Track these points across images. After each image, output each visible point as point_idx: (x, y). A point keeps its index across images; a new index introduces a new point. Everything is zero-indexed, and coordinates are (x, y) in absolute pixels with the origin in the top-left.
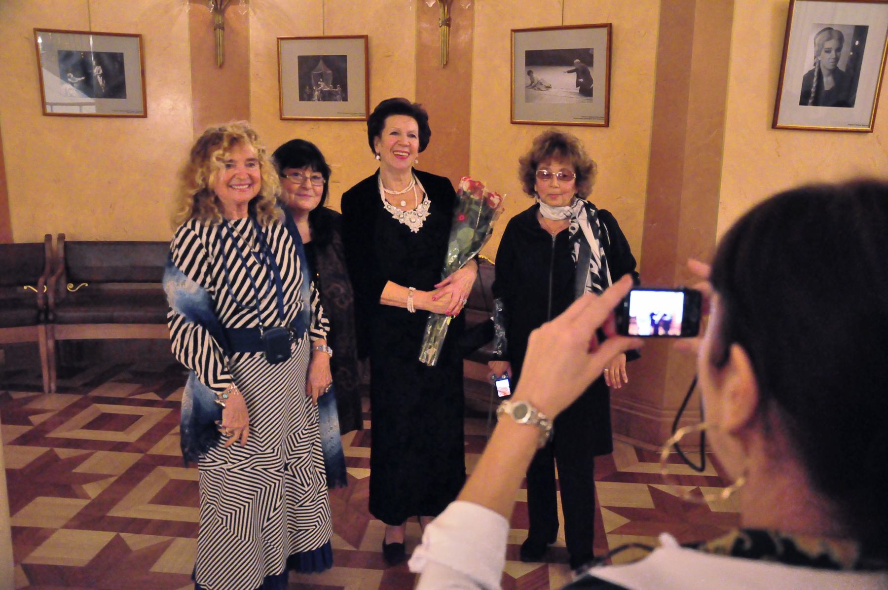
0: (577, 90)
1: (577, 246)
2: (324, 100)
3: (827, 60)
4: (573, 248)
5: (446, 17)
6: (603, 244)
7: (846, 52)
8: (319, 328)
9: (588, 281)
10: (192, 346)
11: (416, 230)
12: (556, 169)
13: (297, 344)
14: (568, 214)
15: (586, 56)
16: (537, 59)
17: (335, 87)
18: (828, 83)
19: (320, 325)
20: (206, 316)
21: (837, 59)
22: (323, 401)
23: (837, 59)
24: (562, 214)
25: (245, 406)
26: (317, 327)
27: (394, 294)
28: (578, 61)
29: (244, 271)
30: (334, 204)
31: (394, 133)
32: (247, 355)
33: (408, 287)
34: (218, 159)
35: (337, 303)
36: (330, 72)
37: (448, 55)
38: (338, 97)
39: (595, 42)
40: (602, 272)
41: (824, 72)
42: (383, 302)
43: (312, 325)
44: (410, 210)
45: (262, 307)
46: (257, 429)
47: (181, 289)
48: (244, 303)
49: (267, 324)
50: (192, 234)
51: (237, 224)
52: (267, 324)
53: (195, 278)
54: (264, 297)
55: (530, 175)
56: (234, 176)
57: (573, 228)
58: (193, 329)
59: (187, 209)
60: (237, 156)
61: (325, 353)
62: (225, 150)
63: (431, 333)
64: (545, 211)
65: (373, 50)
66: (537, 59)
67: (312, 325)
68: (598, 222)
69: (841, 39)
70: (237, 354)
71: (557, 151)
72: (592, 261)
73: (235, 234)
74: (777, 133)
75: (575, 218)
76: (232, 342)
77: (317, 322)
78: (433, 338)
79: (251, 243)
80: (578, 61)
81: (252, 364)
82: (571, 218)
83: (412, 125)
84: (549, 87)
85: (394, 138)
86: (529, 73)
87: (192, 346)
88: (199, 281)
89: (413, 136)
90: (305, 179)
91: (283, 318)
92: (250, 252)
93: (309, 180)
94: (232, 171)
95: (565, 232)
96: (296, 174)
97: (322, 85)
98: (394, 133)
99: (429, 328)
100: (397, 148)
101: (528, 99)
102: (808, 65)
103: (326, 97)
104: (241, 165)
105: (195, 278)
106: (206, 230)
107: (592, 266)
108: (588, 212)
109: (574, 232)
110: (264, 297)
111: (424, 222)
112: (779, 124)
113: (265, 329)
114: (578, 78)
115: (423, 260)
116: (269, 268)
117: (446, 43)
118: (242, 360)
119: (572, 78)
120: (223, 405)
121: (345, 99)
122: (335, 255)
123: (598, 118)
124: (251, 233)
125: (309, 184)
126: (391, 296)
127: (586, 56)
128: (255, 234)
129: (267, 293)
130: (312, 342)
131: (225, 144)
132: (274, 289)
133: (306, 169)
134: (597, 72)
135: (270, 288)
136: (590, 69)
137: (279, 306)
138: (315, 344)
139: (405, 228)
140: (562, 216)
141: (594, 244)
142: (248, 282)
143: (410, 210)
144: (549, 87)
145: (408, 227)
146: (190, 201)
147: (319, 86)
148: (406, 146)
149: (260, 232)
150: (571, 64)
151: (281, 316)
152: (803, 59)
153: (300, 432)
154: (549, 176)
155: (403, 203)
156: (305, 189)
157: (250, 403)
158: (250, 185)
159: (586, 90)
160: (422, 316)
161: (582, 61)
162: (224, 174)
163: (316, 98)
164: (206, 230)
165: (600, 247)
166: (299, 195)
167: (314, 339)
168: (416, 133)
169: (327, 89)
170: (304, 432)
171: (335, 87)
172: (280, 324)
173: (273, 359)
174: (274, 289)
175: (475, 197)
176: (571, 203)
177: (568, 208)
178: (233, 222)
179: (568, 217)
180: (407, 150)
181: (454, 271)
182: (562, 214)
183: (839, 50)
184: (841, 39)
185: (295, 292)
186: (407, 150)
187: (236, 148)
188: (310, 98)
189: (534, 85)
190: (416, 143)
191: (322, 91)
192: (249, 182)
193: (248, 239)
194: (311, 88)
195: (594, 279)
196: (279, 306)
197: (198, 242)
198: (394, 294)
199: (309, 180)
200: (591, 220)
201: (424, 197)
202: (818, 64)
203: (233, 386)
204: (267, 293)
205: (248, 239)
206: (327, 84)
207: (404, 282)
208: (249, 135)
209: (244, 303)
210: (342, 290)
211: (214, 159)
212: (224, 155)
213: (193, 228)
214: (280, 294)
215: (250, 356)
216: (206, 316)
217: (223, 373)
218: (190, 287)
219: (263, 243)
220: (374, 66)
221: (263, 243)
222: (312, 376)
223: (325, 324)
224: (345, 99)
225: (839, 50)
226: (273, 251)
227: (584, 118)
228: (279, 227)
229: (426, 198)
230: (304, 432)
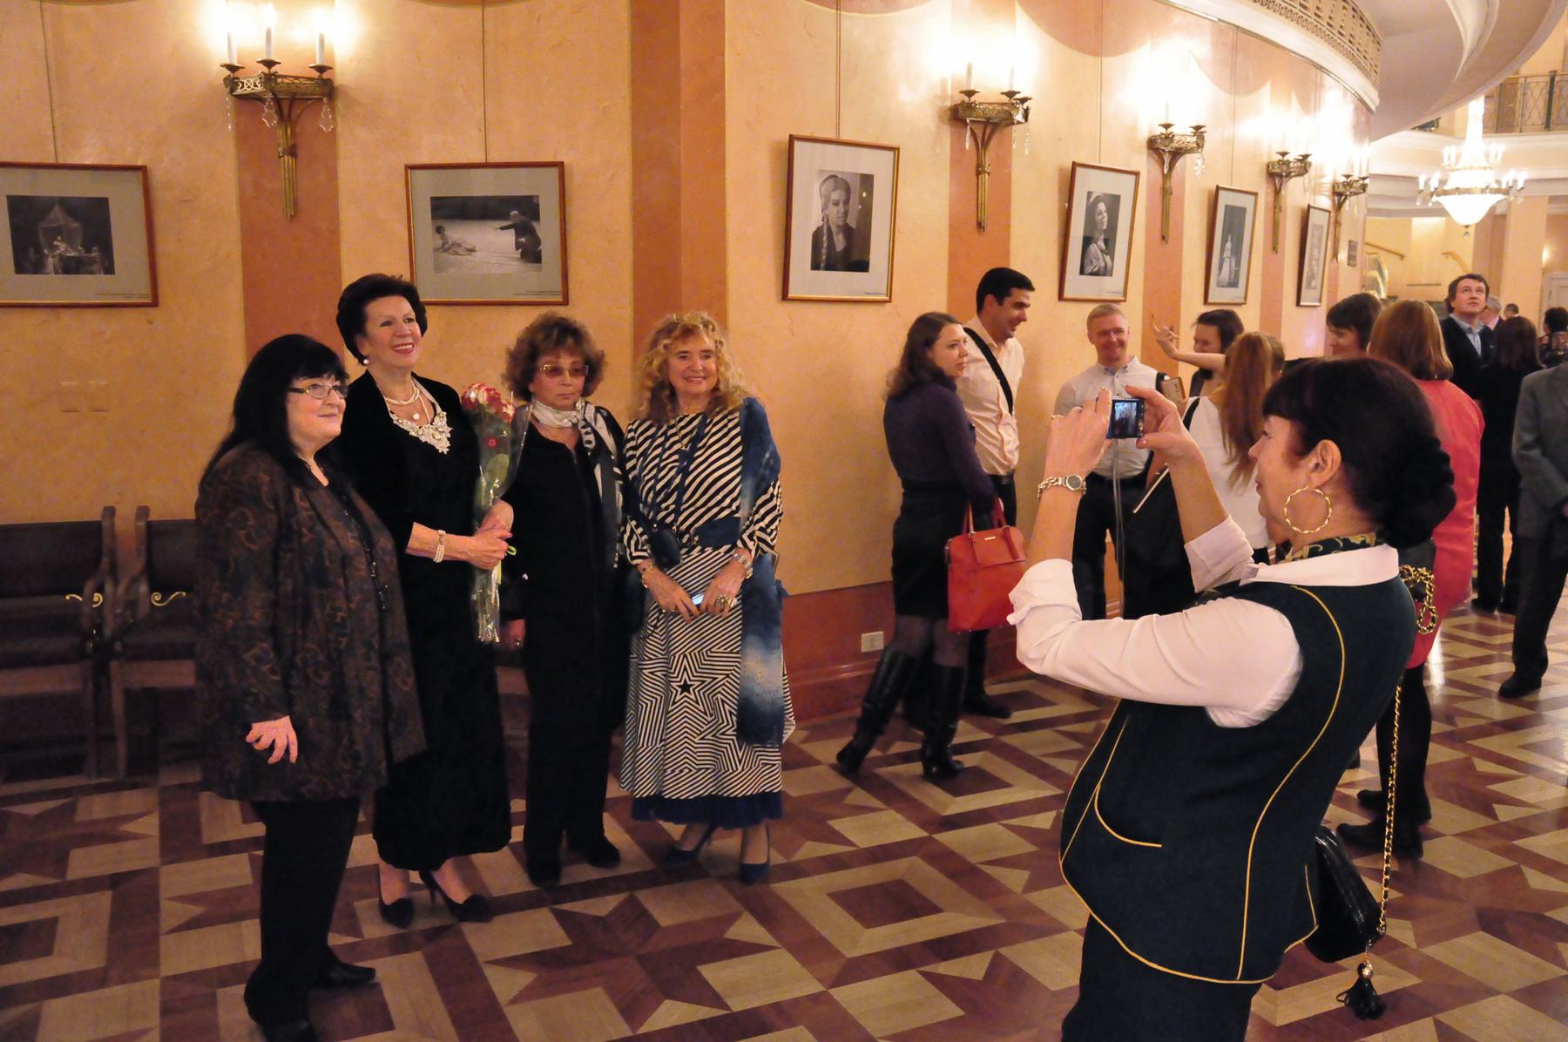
0: (518, 254)
2: (67, 271)
3: (835, 213)
5: (291, 142)
7: (855, 206)
11: (446, 451)
12: (566, 362)
13: (702, 551)
15: (529, 207)
16: (450, 210)
17: (88, 250)
18: (840, 243)
21: (846, 213)
23: (846, 213)
28: (520, 214)
31: (387, 324)
36: (76, 225)
37: (295, 203)
38: (95, 267)
39: (542, 186)
41: (834, 229)
42: (408, 551)
59: (646, 404)
60: (691, 346)
65: (159, 195)
66: (450, 210)
69: (848, 190)
71: (570, 340)
74: (787, 305)
80: (520, 214)
83: (406, 307)
84: (472, 251)
86: (439, 230)
89: (410, 320)
97: (62, 247)
98: (387, 324)
101: (438, 268)
102: (815, 221)
103: (71, 267)
112: (790, 295)
114: (518, 235)
117: (293, 184)
119: (509, 238)
121: (109, 269)
123: (551, 293)
127: (529, 207)
134: (547, 228)
136: (535, 224)
139: (430, 448)
144: (472, 251)
146: (648, 394)
147: (53, 248)
150: (505, 216)
152: (810, 214)
154: (556, 371)
159: (531, 253)
161: (522, 213)
163: (51, 268)
168: (413, 315)
169: (72, 254)
171: (88, 250)
180: (410, 340)
183: (847, 202)
184: (848, 190)
188: (38, 268)
189: (446, 247)
191: (62, 257)
193: (685, 436)
194: (39, 251)
202: (826, 218)
205: (685, 436)
206: (71, 243)
208: (706, 326)
220: (161, 216)
224: (109, 269)
225: (847, 202)
227: (540, 293)
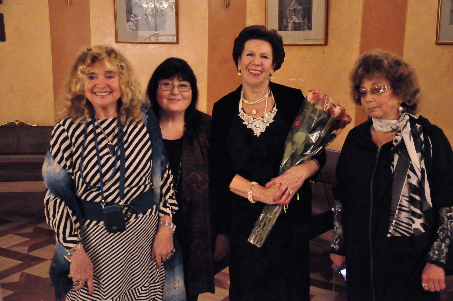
1: (396, 157)
4: (393, 160)
6: (424, 155)
8: (166, 207)
9: (405, 190)
10: (56, 213)
13: (137, 217)
14: (394, 127)
19: (168, 205)
20: (66, 190)
22: (168, 265)
24: (389, 126)
25: (90, 261)
26: (165, 206)
27: (239, 185)
29: (96, 159)
30: (204, 106)
32: (94, 222)
33: (251, 181)
34: (82, 72)
35: (195, 188)
40: (421, 183)
43: (161, 204)
44: (258, 116)
45: (105, 188)
46: (101, 281)
47: (52, 168)
48: (92, 184)
49: (110, 199)
50: (62, 128)
51: (102, 123)
52: (110, 199)
53: (59, 163)
54: (108, 180)
55: (358, 94)
56: (95, 86)
57: (396, 141)
58: (53, 199)
60: (97, 70)
61: (168, 228)
62: (89, 66)
63: (263, 219)
64: (377, 124)
67: (161, 204)
68: (422, 137)
70: (88, 221)
72: (410, 173)
73: (98, 131)
75: (400, 131)
76: (83, 211)
77: (165, 202)
78: (262, 224)
79: (110, 138)
81: (96, 229)
82: (396, 131)
83: (265, 48)
85: (249, 59)
87: (56, 213)
88: (63, 164)
89: (266, 57)
90: (174, 87)
91: (122, 198)
92: (107, 144)
93: (176, 88)
94: (95, 82)
95: (390, 144)
96: (167, 84)
99: (262, 216)
100: (251, 67)
104: (258, 56)
105: (59, 163)
106: (74, 126)
107: (409, 177)
108: (413, 126)
109: (395, 144)
110: (108, 180)
111: (267, 128)
113: (107, 204)
115: (264, 158)
116: (117, 159)
118: (91, 226)
120: (70, 261)
122: (198, 149)
124: (113, 130)
125: (176, 91)
126: (237, 188)
128: (117, 131)
129: (112, 177)
130: (159, 217)
131: (88, 61)
132: (118, 175)
133: (173, 79)
135: (114, 174)
137: (121, 188)
138: (161, 219)
139: (251, 131)
140: (389, 129)
141: (415, 157)
142: (97, 168)
143: (258, 116)
145: (253, 131)
148: (259, 65)
149: (121, 130)
151: (122, 195)
153: (139, 288)
155: (254, 112)
156: (173, 94)
157: (95, 260)
158: (110, 93)
160: (260, 206)
162: (88, 84)
164: (74, 126)
165: (421, 160)
166: (170, 100)
167: (161, 215)
170: (143, 288)
172: (120, 201)
173: (110, 229)
174: (118, 175)
175: (319, 107)
176: (398, 118)
177: (394, 122)
178: (99, 121)
179: (394, 130)
180: (259, 68)
181: (288, 169)
182: (389, 126)
185: (144, 178)
186: (259, 68)
187: (97, 64)
190: (268, 63)
192: (108, 90)
195: (412, 188)
196: (121, 188)
197: (65, 134)
198: (239, 185)
199: (176, 88)
200: (415, 135)
201: (274, 107)
203: (80, 246)
204: (112, 177)
207: (249, 177)
209: (92, 184)
210: (199, 178)
211: (79, 72)
212: (85, 69)
213: (64, 124)
214: (122, 180)
215: (96, 224)
216: (66, 190)
217: (70, 236)
218: (55, 168)
219: (120, 140)
221: (120, 140)
222: (155, 244)
223: (172, 204)
226: (125, 146)
228: (139, 126)
229: (275, 108)
230: (143, 288)
